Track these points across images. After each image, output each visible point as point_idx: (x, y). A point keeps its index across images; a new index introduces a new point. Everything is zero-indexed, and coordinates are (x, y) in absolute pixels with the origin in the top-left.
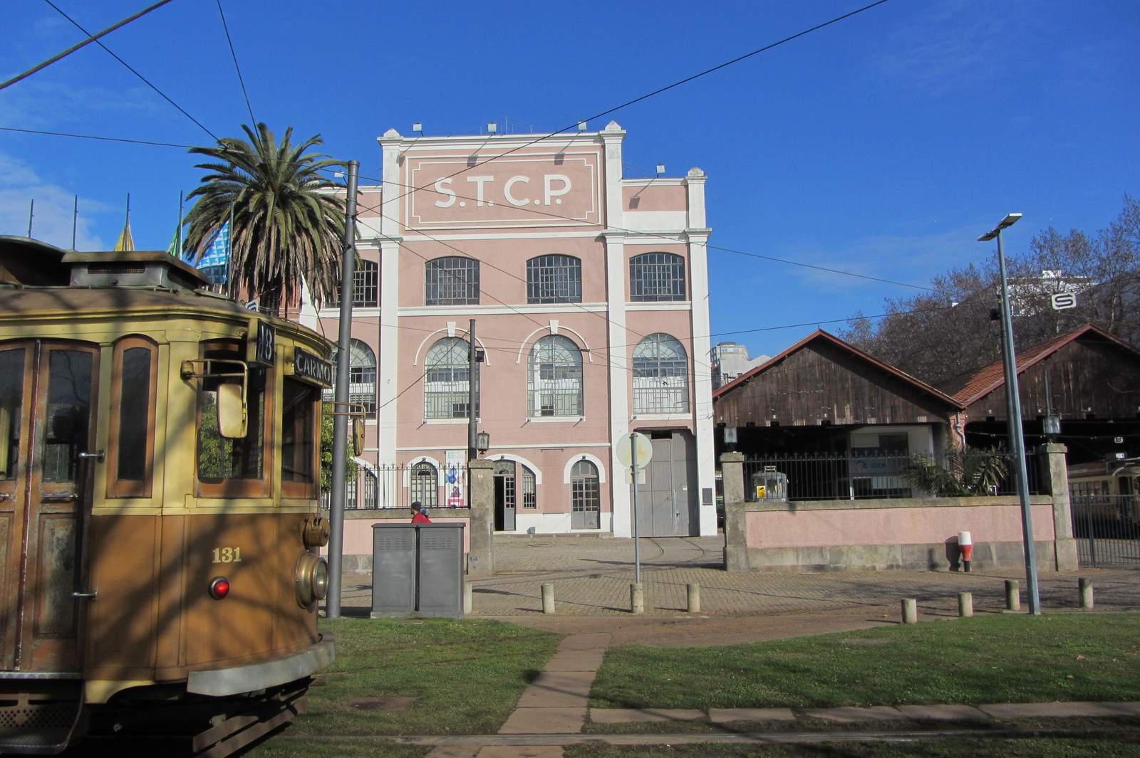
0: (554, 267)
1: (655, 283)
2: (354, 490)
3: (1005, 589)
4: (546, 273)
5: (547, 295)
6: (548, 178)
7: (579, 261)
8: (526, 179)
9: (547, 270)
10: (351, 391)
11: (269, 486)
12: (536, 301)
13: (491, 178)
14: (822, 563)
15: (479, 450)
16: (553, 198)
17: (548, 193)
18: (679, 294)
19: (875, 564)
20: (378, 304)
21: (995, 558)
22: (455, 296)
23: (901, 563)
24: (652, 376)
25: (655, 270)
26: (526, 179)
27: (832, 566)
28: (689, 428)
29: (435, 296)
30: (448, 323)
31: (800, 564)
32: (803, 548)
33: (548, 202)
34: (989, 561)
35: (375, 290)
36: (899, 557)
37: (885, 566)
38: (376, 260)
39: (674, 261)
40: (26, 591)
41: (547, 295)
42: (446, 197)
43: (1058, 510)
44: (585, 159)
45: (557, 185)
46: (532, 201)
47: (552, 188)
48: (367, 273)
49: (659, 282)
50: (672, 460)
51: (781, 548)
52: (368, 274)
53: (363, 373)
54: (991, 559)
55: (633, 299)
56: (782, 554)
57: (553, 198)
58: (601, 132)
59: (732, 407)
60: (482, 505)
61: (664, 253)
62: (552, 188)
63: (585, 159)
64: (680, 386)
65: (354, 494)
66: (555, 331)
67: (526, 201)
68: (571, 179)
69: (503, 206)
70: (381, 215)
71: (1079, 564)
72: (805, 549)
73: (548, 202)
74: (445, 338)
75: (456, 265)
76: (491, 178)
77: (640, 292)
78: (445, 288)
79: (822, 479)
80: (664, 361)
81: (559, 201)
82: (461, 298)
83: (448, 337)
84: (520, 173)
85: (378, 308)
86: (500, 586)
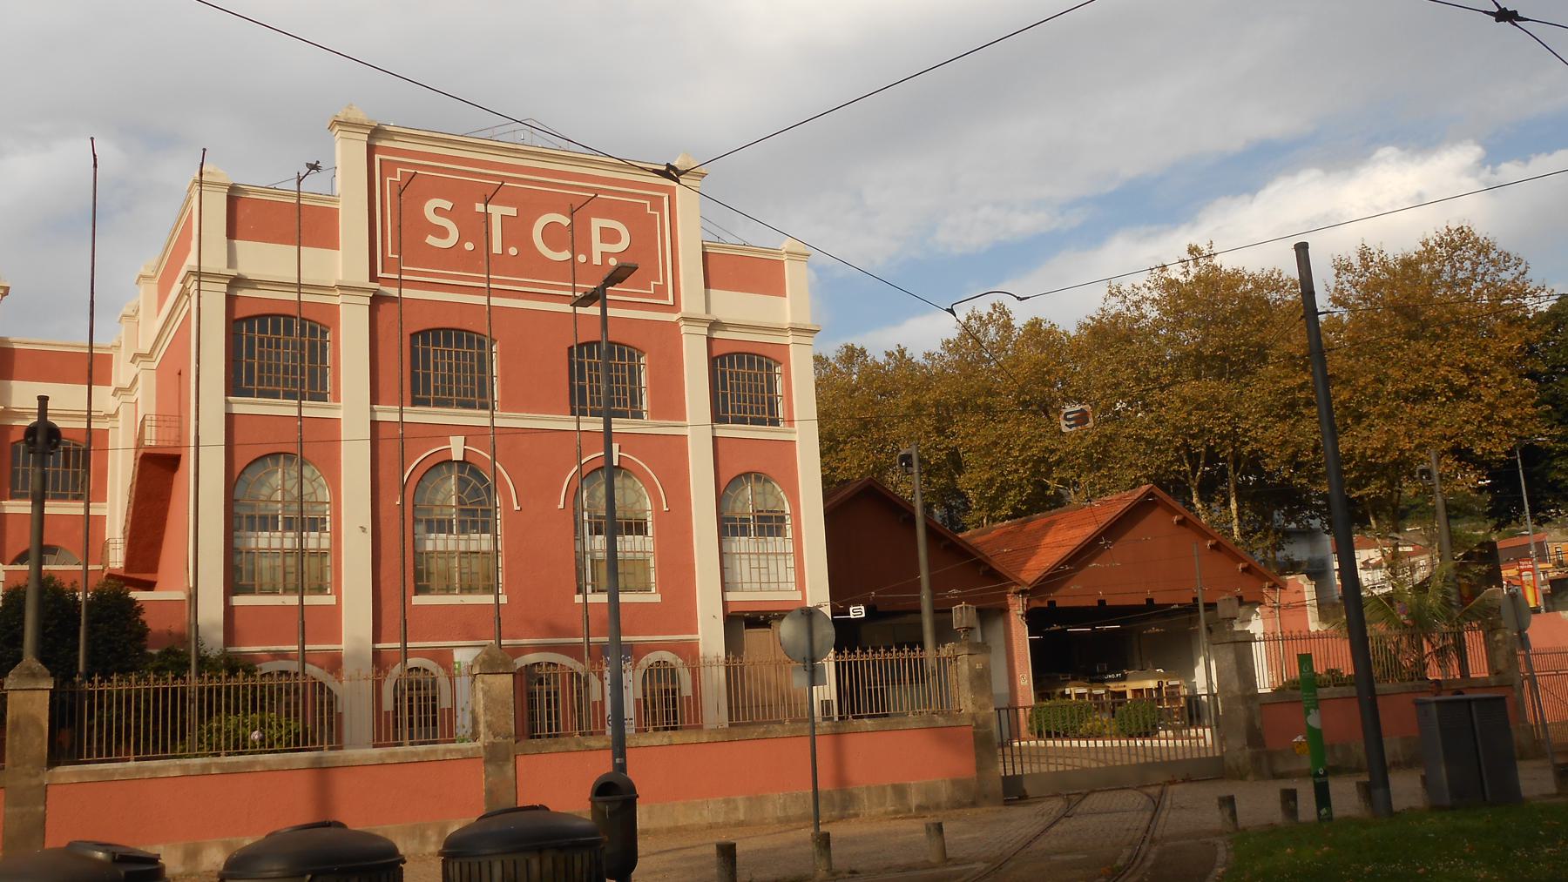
3: (1389, 775)
9: (617, 365)
11: (1232, 645)
12: (426, 403)
13: (512, 212)
16: (605, 255)
17: (598, 247)
22: (458, 394)
24: (773, 536)
25: (450, 357)
29: (427, 390)
33: (597, 260)
44: (649, 212)
45: (610, 236)
48: (479, 354)
53: (479, 519)
57: (605, 255)
61: (452, 329)
63: (649, 212)
69: (531, 263)
73: (597, 260)
76: (512, 212)
78: (443, 381)
80: (761, 514)
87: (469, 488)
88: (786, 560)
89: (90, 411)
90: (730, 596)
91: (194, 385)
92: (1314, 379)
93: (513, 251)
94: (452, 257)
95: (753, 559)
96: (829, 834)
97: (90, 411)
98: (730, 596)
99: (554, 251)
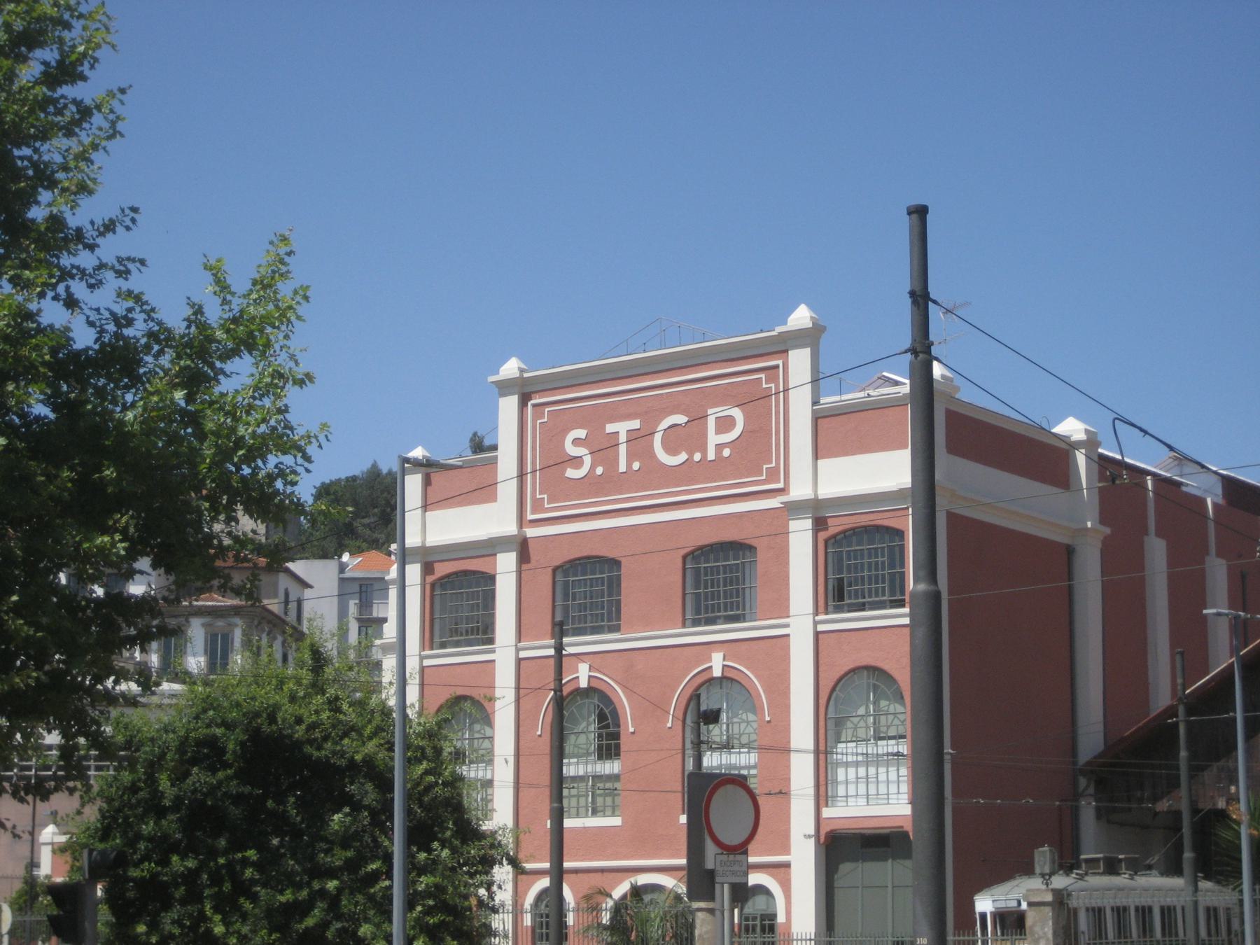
2: (900, 802)
8: (680, 419)
13: (635, 424)
16: (719, 447)
17: (713, 439)
26: (680, 419)
33: (711, 455)
40: (577, 910)
42: (576, 461)
44: (765, 467)
45: (725, 424)
47: (719, 431)
50: (890, 889)
57: (719, 447)
59: (501, 928)
62: (719, 431)
63: (765, 467)
64: (852, 771)
65: (895, 802)
69: (655, 475)
73: (711, 455)
75: (586, 586)
76: (635, 424)
79: (1166, 912)
87: (672, 713)
88: (888, 772)
89: (867, 775)
90: (827, 813)
91: (1181, 923)
92: (32, 871)
93: (636, 466)
94: (591, 485)
95: (872, 782)
96: (628, 431)
97: (867, 775)
98: (827, 813)
99: (666, 452)
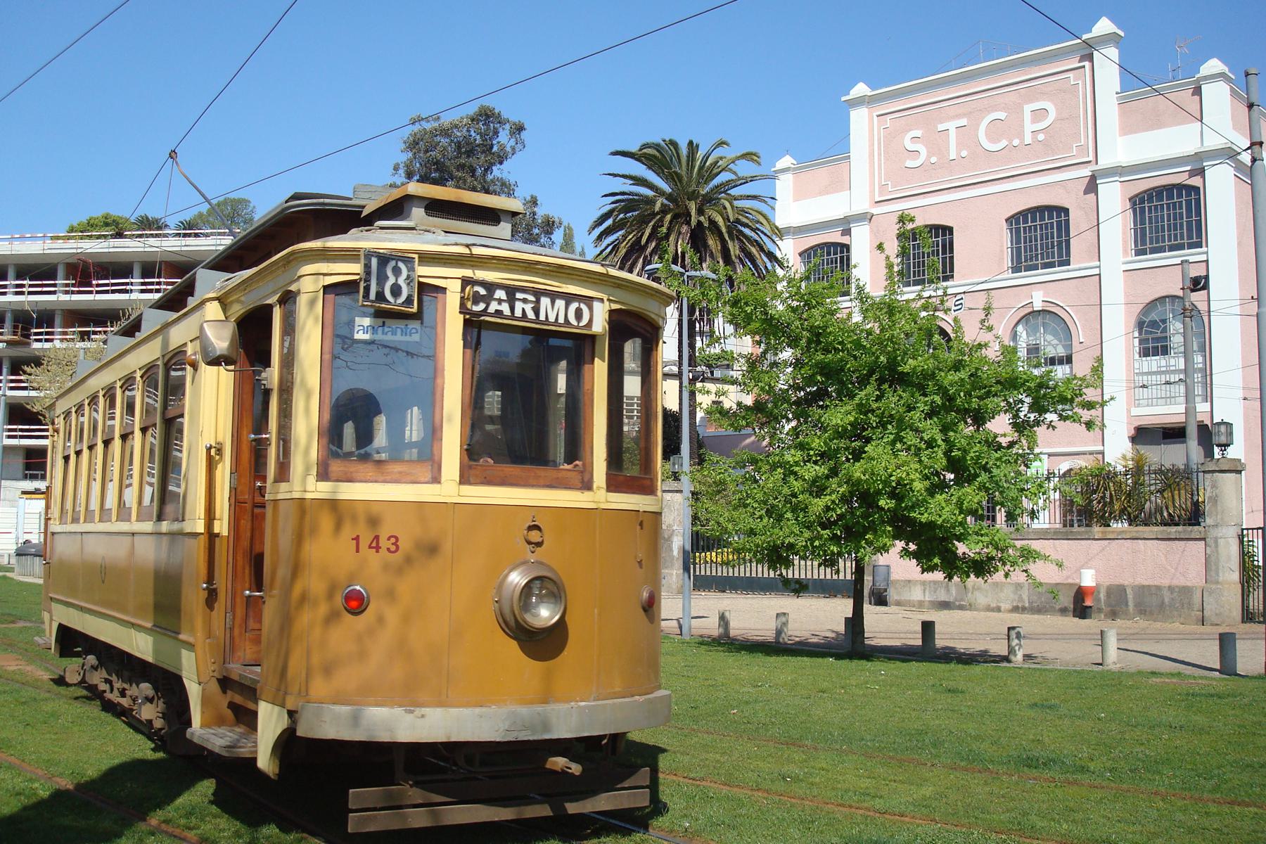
0: (940, 239)
1: (1163, 226)
4: (1047, 229)
5: (1176, 239)
6: (1028, 109)
7: (1066, 211)
8: (1002, 115)
9: (1156, 207)
10: (1182, 361)
13: (963, 122)
14: (947, 600)
15: (1218, 446)
17: (1029, 127)
18: (1195, 240)
19: (1002, 605)
20: (1204, 244)
21: (1131, 604)
23: (1027, 605)
27: (957, 603)
28: (1205, 423)
30: (1034, 293)
31: (927, 599)
32: (930, 582)
33: (1028, 140)
34: (1124, 608)
35: (1199, 223)
36: (1025, 597)
37: (1011, 607)
38: (848, 243)
39: (1188, 195)
41: (919, 276)
43: (1210, 547)
45: (1040, 114)
46: (1011, 141)
47: (1034, 121)
49: (1169, 226)
51: (909, 581)
52: (842, 258)
54: (1127, 605)
55: (1139, 253)
56: (910, 588)
58: (1085, 37)
60: (670, 526)
62: (1034, 121)
66: (1038, 306)
67: (1004, 143)
68: (1056, 105)
70: (1201, 121)
71: (1084, 618)
72: (932, 584)
74: (1029, 313)
76: (963, 122)
77: (1144, 243)
81: (1041, 137)
82: (1051, 260)
83: (1034, 312)
84: (994, 108)
85: (1204, 249)
86: (1124, 626)
